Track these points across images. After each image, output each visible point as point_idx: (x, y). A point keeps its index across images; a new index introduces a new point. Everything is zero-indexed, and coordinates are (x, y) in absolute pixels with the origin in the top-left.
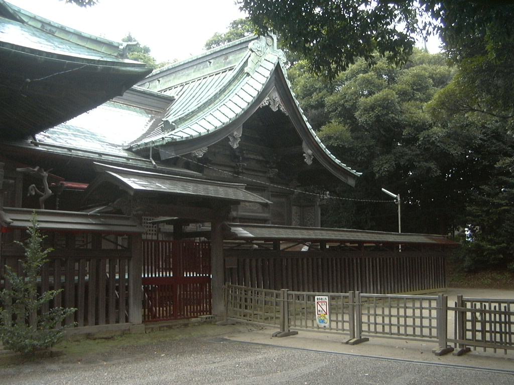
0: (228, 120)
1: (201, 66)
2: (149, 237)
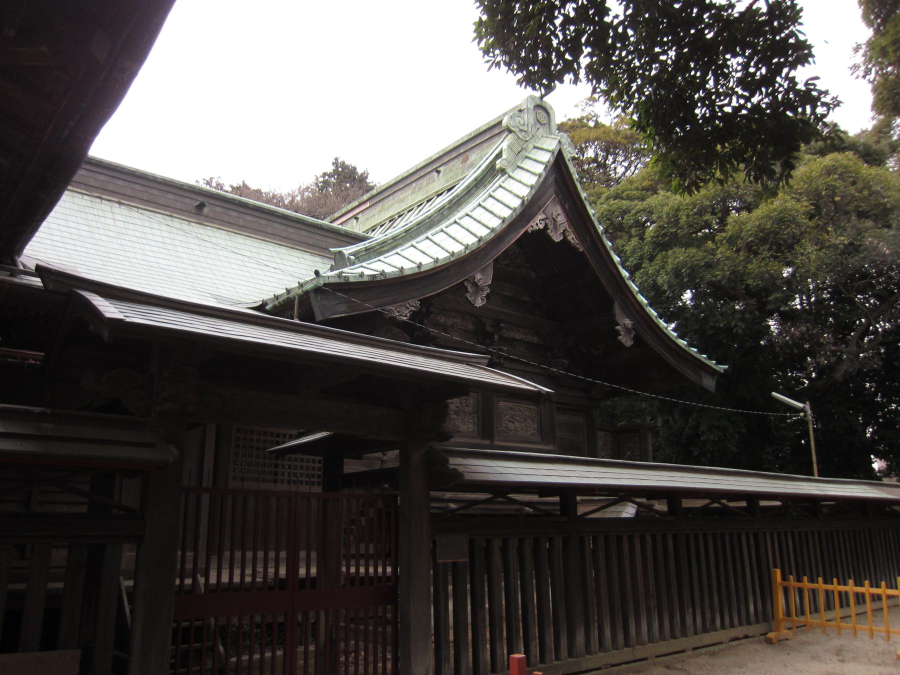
0: (462, 248)
1: (424, 181)
2: (304, 489)
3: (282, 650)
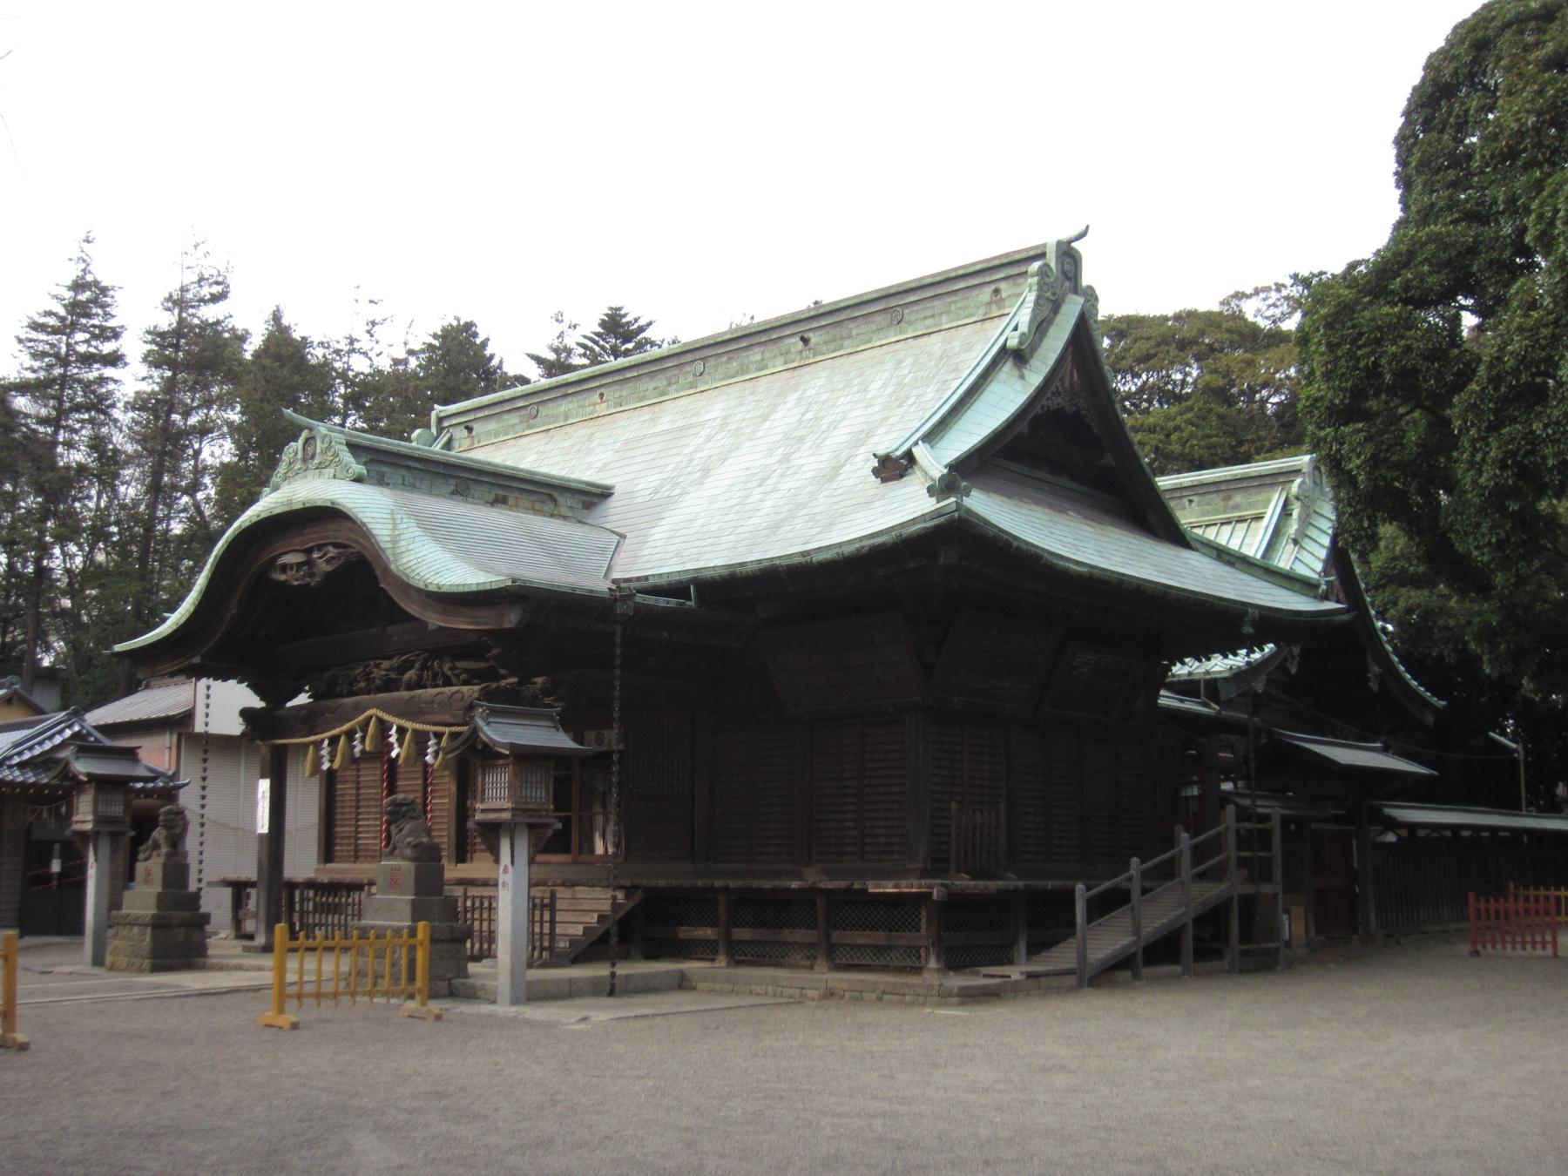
3: (248, 890)
